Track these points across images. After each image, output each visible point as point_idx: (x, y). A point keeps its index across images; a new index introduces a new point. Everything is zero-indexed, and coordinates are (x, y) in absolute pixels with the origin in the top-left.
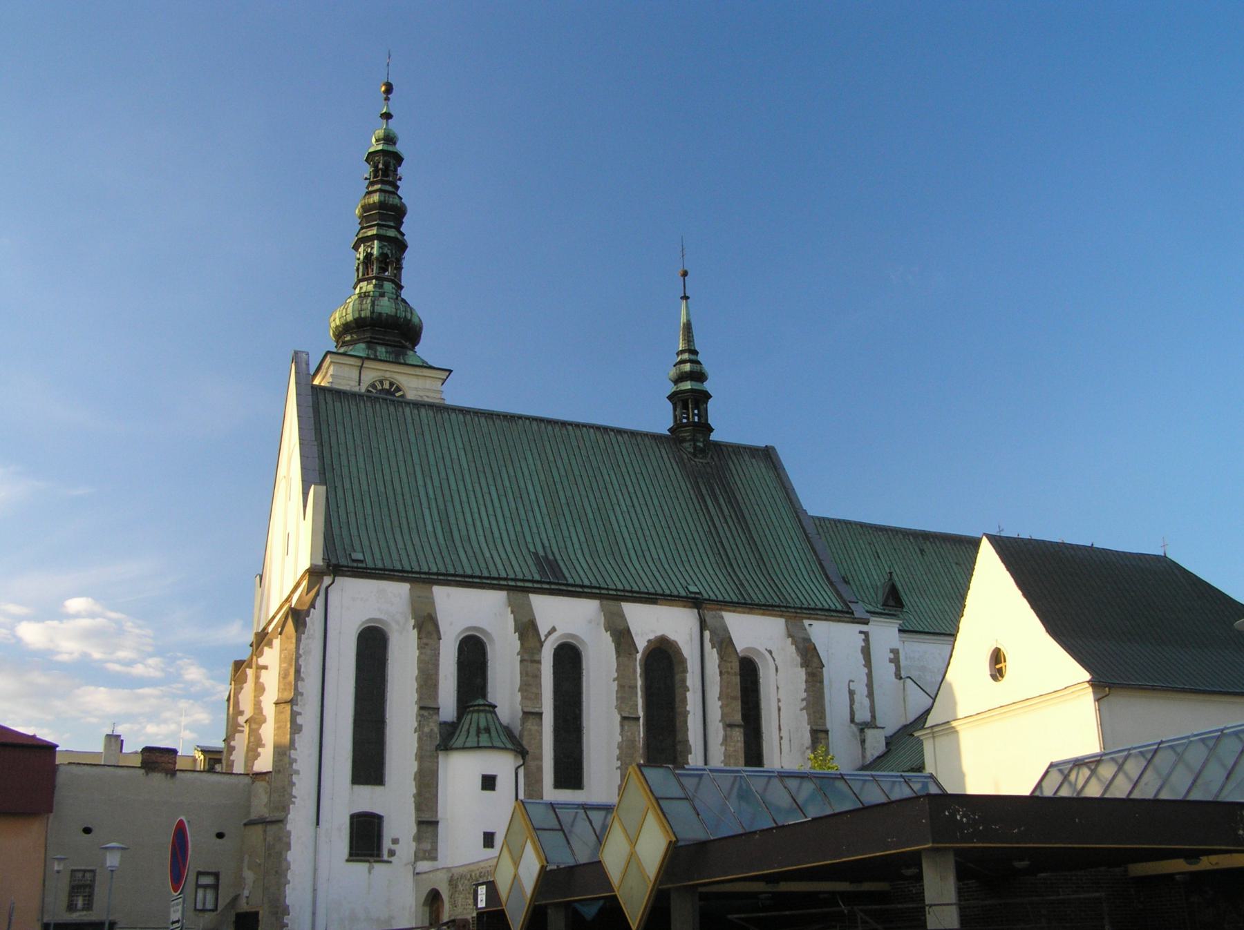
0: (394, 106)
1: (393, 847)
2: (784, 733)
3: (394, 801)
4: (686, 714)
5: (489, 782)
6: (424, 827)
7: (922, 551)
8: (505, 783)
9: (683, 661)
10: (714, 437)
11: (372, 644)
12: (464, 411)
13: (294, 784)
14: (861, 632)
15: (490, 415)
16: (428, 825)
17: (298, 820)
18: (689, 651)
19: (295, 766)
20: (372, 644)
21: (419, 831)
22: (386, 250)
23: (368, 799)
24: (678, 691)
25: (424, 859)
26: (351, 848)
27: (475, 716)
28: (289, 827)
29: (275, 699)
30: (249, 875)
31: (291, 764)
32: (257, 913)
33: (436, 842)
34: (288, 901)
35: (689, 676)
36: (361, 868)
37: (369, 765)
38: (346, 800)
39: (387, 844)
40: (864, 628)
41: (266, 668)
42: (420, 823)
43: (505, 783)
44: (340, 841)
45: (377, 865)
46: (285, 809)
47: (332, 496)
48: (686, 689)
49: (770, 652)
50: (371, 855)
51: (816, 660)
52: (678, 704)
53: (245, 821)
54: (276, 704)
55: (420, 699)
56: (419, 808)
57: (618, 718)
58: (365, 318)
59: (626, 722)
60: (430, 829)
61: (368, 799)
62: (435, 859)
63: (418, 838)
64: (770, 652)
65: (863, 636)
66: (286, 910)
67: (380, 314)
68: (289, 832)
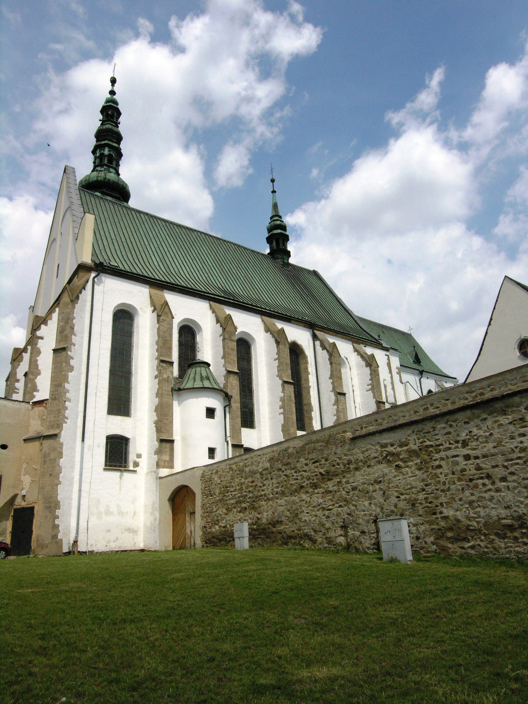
0: (116, 89)
1: (138, 460)
2: (357, 405)
3: (139, 429)
4: (309, 388)
5: (210, 413)
6: (164, 444)
7: (383, 332)
8: (219, 413)
9: (305, 357)
10: (291, 261)
11: (123, 318)
12: (165, 221)
13: (66, 408)
14: (386, 355)
15: (179, 226)
16: (165, 443)
17: (69, 433)
18: (309, 352)
19: (68, 395)
20: (123, 318)
21: (160, 446)
22: (111, 153)
23: (118, 425)
24: (303, 375)
25: (164, 467)
26: (106, 461)
27: (198, 369)
28: (62, 440)
29: (54, 347)
30: (27, 480)
31: (65, 393)
32: (32, 509)
33: (173, 451)
34: (59, 498)
35: (309, 365)
36: (115, 475)
37: (120, 402)
38: (105, 425)
39: (132, 457)
40: (387, 353)
41: (42, 338)
42: (162, 441)
43: (219, 413)
44: (99, 453)
45: (126, 474)
46: (59, 426)
47: (98, 218)
48: (308, 373)
49: (347, 359)
50: (120, 466)
51: (374, 362)
52: (303, 382)
53: (24, 438)
54: (55, 351)
55: (160, 355)
56: (159, 430)
57: (281, 382)
58: (100, 181)
59: (286, 385)
60: (168, 445)
61: (118, 425)
62: (172, 467)
63: (158, 452)
64: (347, 359)
65: (387, 357)
66: (57, 505)
67: (109, 180)
68: (62, 444)
